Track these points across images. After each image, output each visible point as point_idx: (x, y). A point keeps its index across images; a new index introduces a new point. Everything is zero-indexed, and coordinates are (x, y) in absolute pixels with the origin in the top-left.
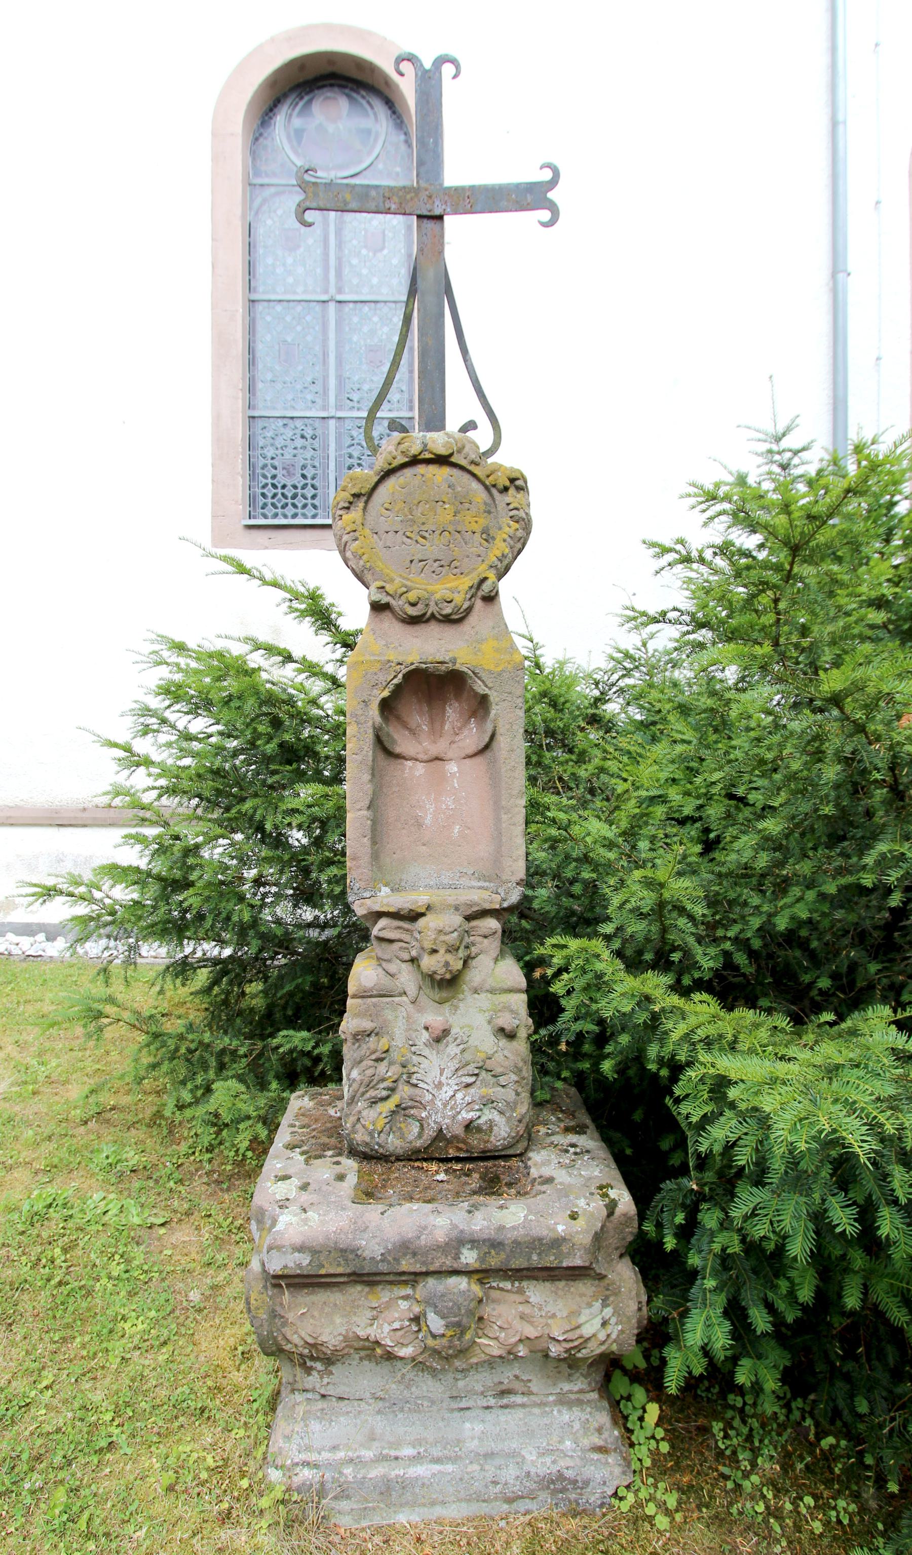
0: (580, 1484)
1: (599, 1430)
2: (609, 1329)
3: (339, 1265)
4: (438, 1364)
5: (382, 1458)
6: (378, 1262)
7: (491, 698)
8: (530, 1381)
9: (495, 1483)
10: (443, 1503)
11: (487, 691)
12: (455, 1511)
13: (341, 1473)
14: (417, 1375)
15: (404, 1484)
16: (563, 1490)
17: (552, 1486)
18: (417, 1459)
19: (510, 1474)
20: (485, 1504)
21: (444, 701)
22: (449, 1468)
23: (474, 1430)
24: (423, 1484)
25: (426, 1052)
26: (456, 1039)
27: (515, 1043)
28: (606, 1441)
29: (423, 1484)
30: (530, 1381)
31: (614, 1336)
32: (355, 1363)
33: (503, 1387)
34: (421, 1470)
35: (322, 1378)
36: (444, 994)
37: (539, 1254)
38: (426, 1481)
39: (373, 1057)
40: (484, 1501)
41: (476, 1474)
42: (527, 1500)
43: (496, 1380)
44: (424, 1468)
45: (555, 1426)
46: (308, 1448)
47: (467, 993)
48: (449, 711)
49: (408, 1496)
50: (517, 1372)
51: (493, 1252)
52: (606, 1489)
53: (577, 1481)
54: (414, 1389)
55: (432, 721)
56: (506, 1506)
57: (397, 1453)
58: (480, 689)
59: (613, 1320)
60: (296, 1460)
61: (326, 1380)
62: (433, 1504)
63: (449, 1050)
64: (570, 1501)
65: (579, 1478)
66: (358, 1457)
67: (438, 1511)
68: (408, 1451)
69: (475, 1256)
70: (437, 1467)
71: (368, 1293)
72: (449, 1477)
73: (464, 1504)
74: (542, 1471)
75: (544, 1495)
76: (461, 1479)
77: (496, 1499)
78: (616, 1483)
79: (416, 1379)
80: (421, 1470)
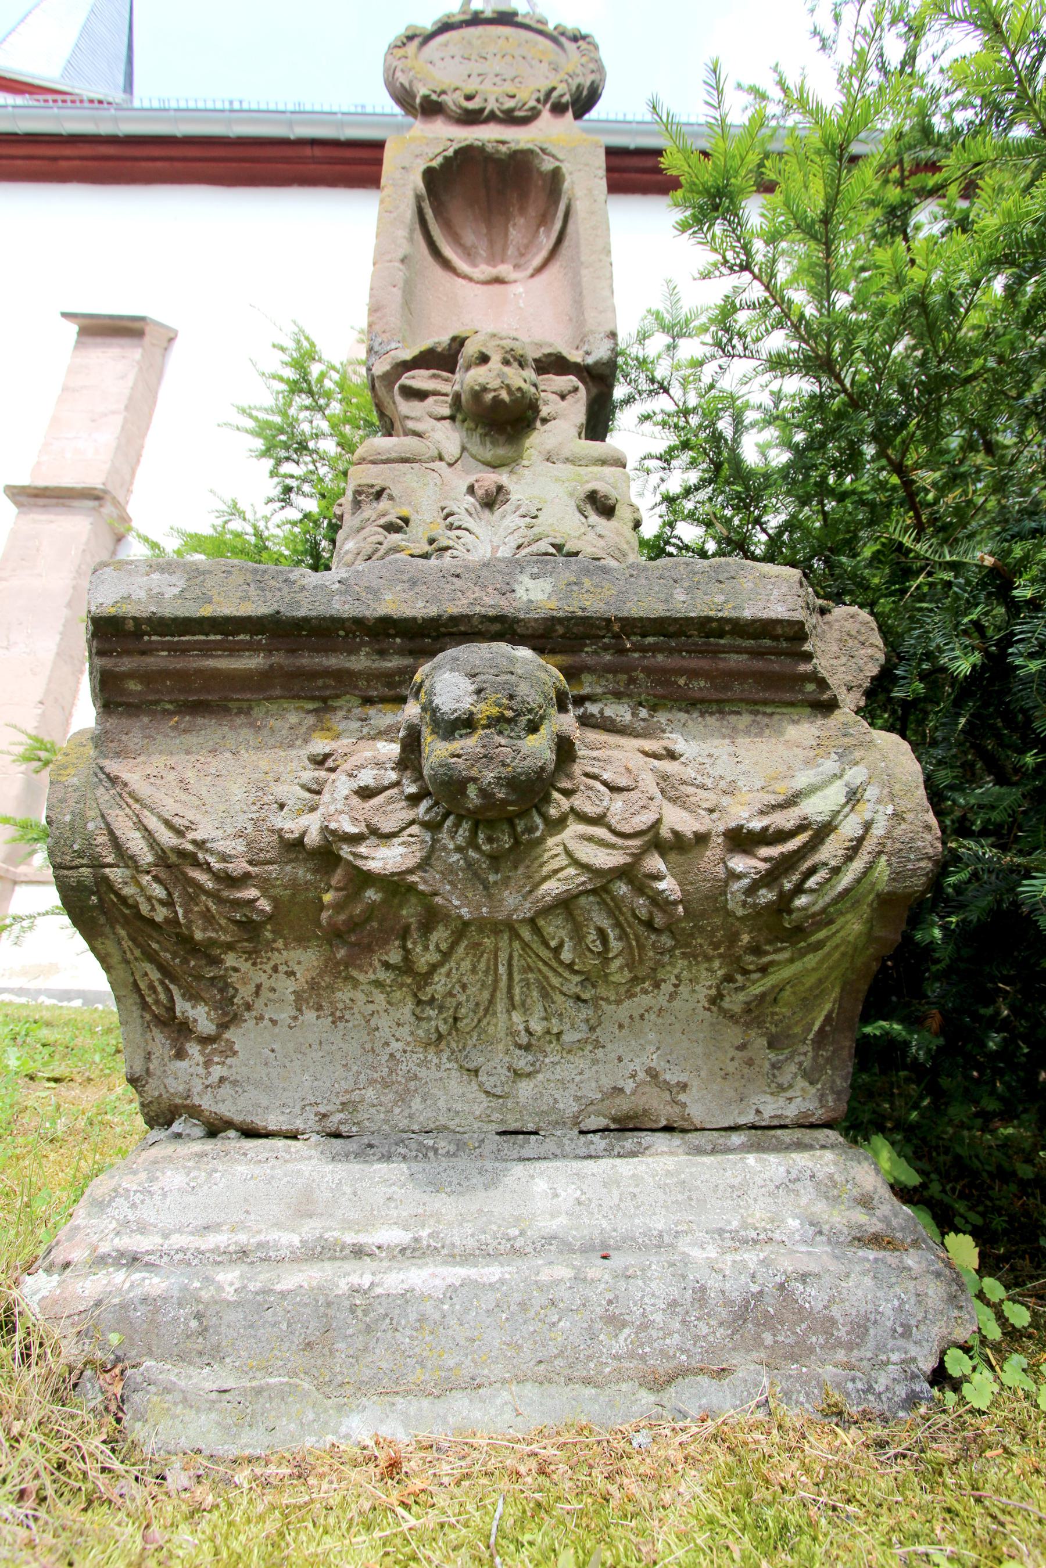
0: (842, 1333)
1: (866, 1202)
2: (865, 811)
3: (246, 598)
4: (466, 901)
5: (319, 1251)
6: (332, 594)
7: (564, 170)
8: (684, 1087)
9: (615, 1322)
10: (475, 1385)
11: (557, 164)
12: (500, 1416)
13: (208, 1280)
14: (424, 1063)
15: (371, 1315)
16: (797, 1353)
17: (768, 1338)
18: (410, 1252)
19: (654, 1289)
20: (590, 1391)
21: (507, 217)
22: (492, 1272)
23: (557, 1192)
24: (422, 1319)
25: (469, 522)
26: (518, 507)
27: (613, 523)
28: (885, 1220)
29: (422, 1319)
30: (684, 1087)
31: (878, 830)
32: (284, 1016)
33: (623, 1105)
34: (422, 1278)
35: (208, 1064)
36: (501, 451)
37: (688, 591)
38: (428, 1307)
39: (382, 521)
40: (587, 1381)
41: (562, 1292)
42: (704, 1380)
43: (607, 1083)
44: (425, 1272)
45: (753, 1192)
46: (142, 1228)
47: (538, 424)
48: (513, 233)
49: (381, 1358)
50: (655, 1061)
51: (587, 583)
52: (913, 1351)
53: (833, 1322)
54: (416, 1103)
55: (491, 243)
56: (647, 1398)
57: (362, 1239)
58: (548, 165)
59: (872, 792)
60: (104, 1248)
61: (217, 1071)
62: (446, 1386)
63: (507, 522)
64: (821, 1385)
65: (836, 1312)
66: (260, 1245)
67: (461, 1408)
68: (394, 1236)
69: (549, 588)
70: (457, 1273)
71: (312, 729)
72: (492, 1297)
73: (530, 1390)
74: (736, 1287)
75: (746, 1367)
76: (523, 1306)
77: (621, 1376)
78: (936, 1331)
79: (423, 1073)
80: (422, 1278)
